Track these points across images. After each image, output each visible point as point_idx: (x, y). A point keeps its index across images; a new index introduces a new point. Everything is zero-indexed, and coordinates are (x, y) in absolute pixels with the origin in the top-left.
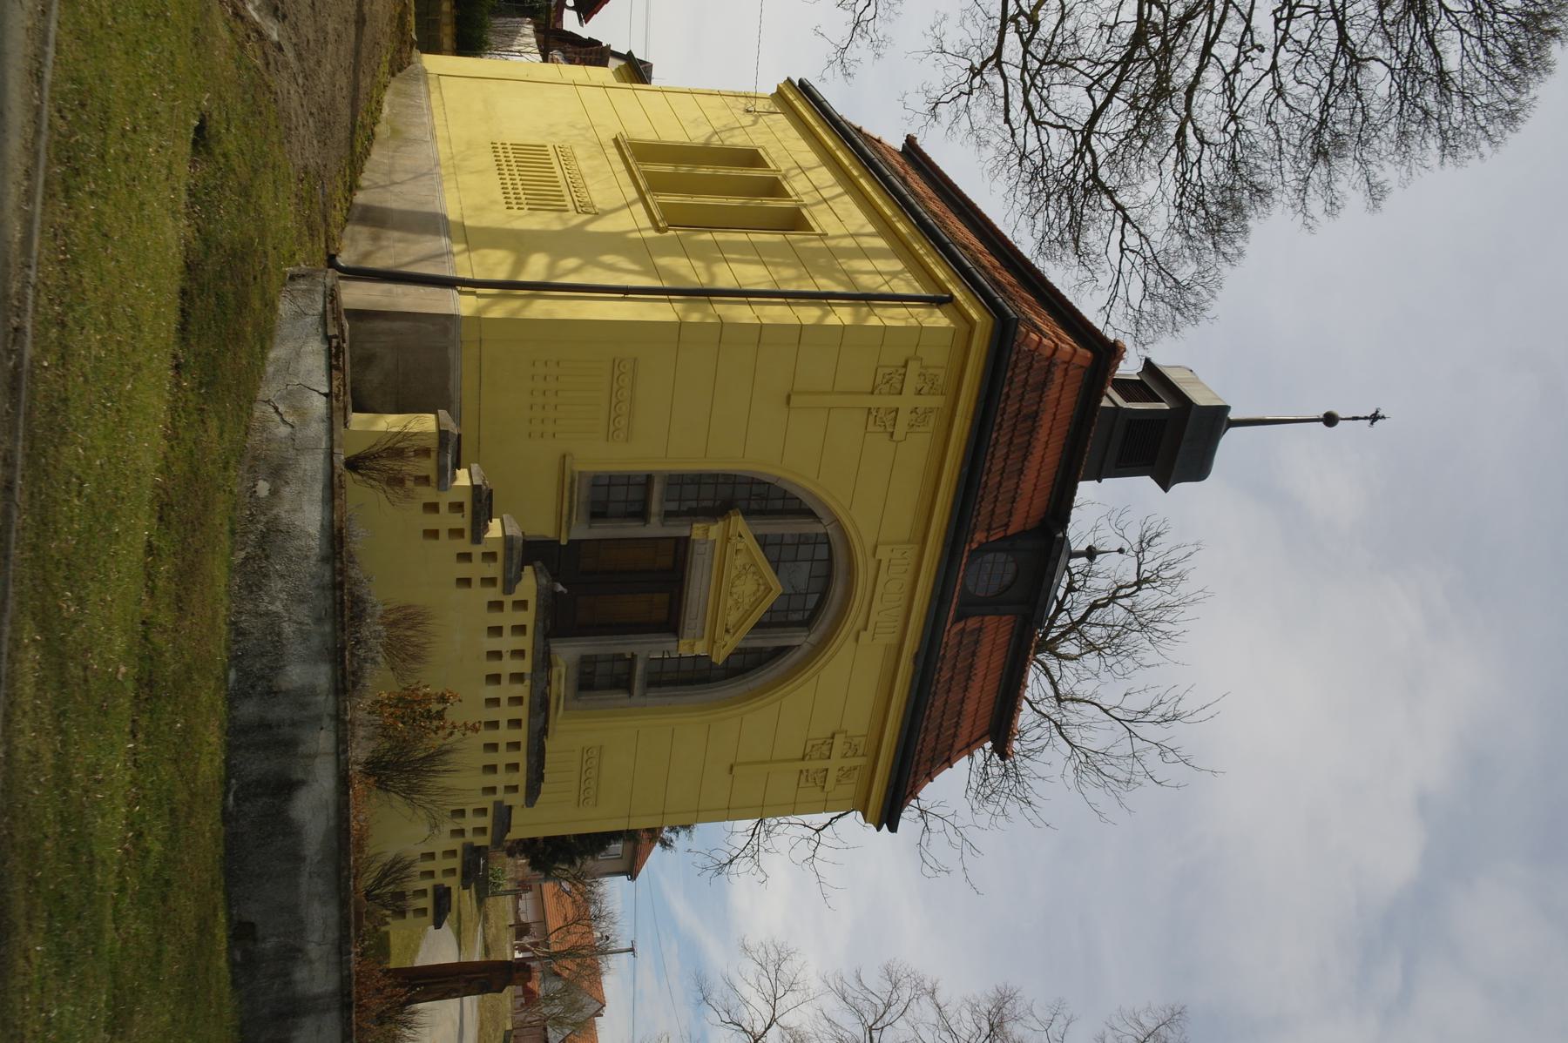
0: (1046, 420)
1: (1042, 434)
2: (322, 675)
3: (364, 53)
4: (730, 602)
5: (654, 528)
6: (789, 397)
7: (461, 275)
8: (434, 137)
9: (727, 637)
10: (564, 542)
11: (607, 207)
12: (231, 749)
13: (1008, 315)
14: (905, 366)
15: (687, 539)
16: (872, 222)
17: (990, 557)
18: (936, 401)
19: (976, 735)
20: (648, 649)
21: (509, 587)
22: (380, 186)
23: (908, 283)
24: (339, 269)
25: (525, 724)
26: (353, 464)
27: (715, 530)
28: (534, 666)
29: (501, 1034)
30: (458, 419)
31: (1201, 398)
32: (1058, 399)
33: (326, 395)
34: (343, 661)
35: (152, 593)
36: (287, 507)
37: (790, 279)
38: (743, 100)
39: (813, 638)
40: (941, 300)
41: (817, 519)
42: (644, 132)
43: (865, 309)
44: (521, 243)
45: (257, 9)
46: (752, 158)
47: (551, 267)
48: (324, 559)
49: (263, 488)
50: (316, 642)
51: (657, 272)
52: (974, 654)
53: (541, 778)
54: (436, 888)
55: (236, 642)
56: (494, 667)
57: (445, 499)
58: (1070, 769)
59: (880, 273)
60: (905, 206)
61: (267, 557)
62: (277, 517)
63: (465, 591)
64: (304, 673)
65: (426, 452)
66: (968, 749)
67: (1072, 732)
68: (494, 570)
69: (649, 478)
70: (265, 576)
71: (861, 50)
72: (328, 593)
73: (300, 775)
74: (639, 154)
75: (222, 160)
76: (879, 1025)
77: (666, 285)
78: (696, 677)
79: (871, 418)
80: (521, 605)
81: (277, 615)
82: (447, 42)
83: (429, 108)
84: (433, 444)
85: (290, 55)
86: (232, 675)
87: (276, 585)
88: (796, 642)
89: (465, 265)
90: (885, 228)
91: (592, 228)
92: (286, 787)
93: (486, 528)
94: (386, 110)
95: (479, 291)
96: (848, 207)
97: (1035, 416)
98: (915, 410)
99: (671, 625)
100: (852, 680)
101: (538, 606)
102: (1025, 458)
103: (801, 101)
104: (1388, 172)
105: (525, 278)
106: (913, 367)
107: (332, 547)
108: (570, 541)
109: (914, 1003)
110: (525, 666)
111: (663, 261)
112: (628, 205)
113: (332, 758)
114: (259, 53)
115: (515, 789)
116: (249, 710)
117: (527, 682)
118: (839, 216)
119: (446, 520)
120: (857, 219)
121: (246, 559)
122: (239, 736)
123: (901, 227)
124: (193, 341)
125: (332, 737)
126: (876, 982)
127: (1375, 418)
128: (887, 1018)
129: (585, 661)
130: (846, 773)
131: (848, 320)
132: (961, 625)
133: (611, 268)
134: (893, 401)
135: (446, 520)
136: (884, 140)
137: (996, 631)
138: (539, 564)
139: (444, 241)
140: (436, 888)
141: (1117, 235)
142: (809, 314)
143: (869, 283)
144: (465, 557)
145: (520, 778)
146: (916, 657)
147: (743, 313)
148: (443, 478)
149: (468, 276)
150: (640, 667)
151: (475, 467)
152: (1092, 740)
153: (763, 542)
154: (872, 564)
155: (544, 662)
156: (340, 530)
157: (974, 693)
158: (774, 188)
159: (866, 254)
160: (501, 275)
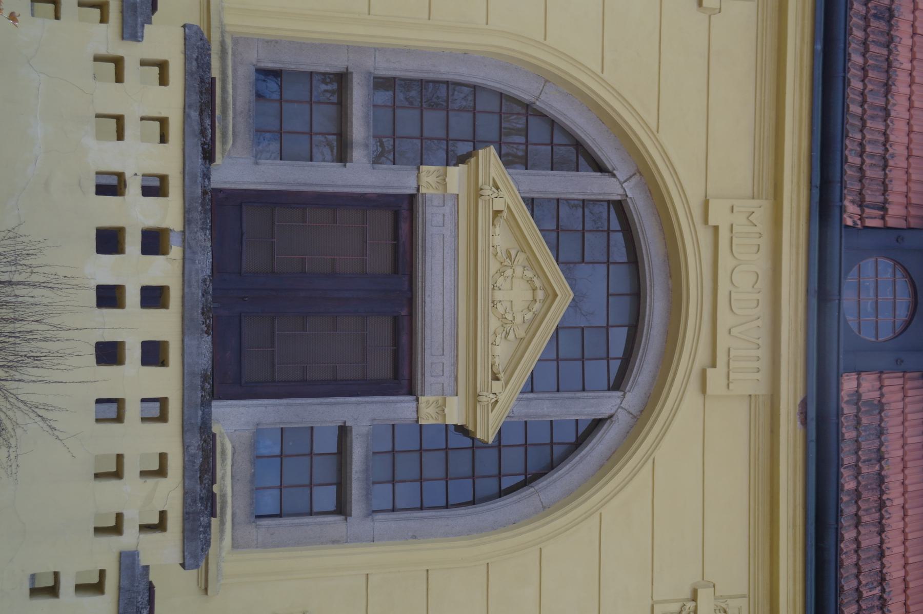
4: (494, 324)
5: (361, 175)
9: (497, 386)
14: (694, 599)
39: (632, 397)
69: (342, 79)
99: (402, 379)
117: (176, 251)
129: (259, 433)
145: (169, 494)
154: (705, 237)
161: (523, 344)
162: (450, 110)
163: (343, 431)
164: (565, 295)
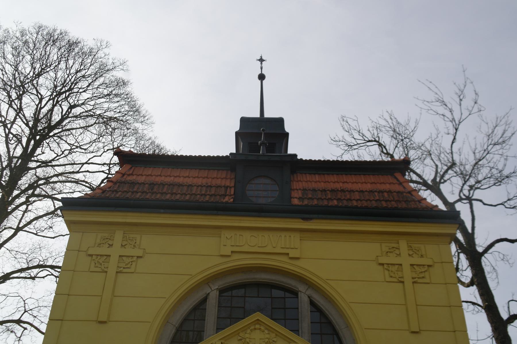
14: (383, 264)
19: (395, 181)
32: (390, 184)
39: (301, 287)
41: (204, 300)
79: (125, 270)
97: (152, 185)
98: (111, 246)
106: (384, 260)
127: (261, 60)
134: (114, 260)
137: (303, 182)
146: (304, 219)
153: (219, 329)
154: (236, 257)
161: (278, 334)
164: (258, 316)
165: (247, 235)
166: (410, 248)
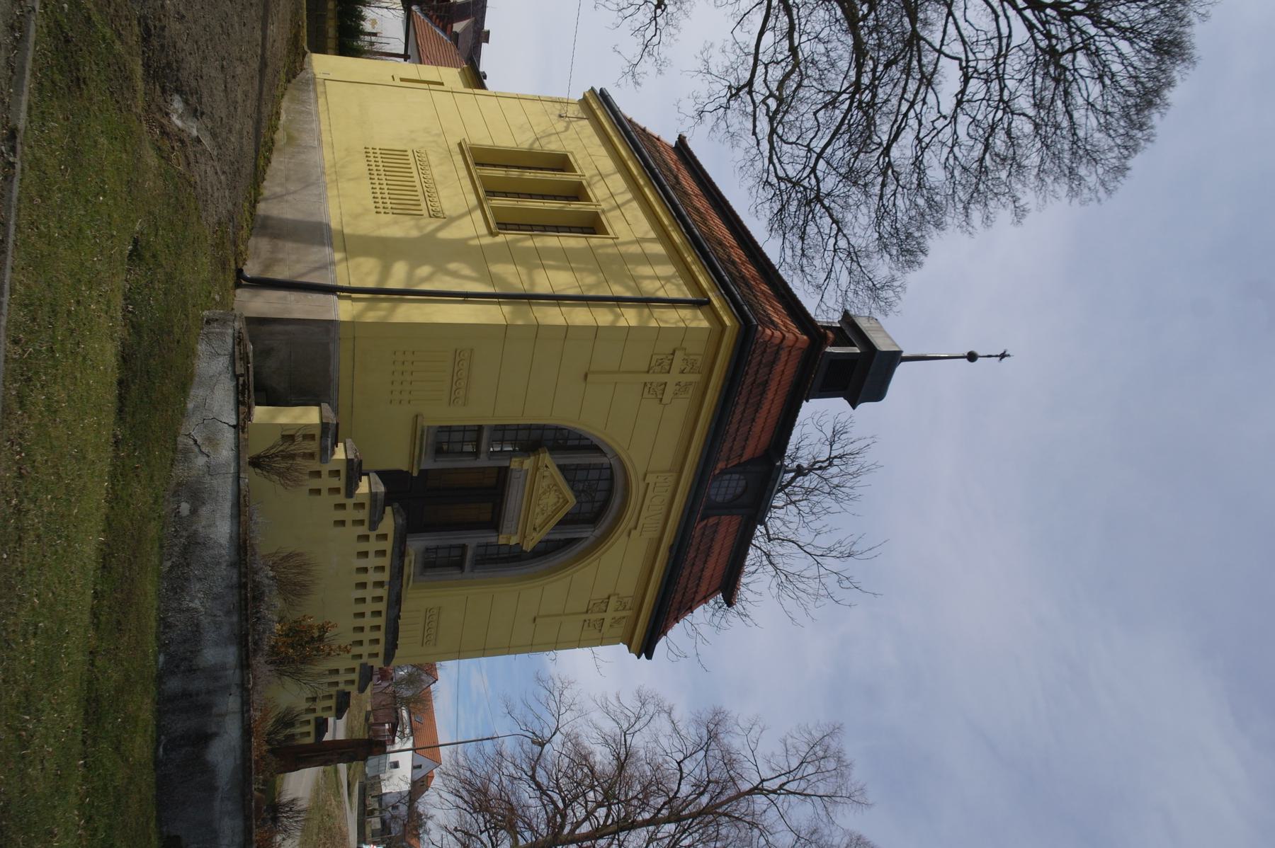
0: (773, 386)
1: (770, 395)
2: (230, 655)
3: (268, 46)
4: (538, 510)
6: (586, 376)
7: (340, 284)
8: (320, 141)
9: (534, 534)
10: (415, 474)
11: (454, 214)
12: (160, 714)
13: (751, 322)
14: (673, 354)
15: (507, 468)
16: (653, 228)
17: (728, 477)
18: (694, 377)
20: (473, 541)
21: (373, 526)
22: (280, 203)
23: (678, 286)
24: (246, 279)
25: (384, 614)
26: (256, 462)
27: (528, 463)
28: (391, 577)
29: (363, 714)
30: (336, 411)
31: (882, 345)
33: (234, 427)
34: (247, 645)
35: (97, 627)
36: (204, 523)
37: (588, 283)
38: (557, 106)
39: (598, 532)
40: (701, 303)
41: (605, 455)
42: (482, 138)
43: (646, 311)
44: (385, 250)
45: (180, 117)
46: (562, 163)
47: (410, 274)
48: (232, 565)
49: (185, 508)
50: (225, 630)
51: (491, 278)
52: (712, 540)
53: (396, 646)
54: (317, 719)
55: (164, 633)
56: (362, 578)
57: (325, 469)
58: (774, 584)
59: (658, 278)
60: (679, 218)
61: (188, 565)
62: (196, 532)
63: (340, 529)
64: (217, 654)
65: (312, 437)
66: (705, 599)
67: (776, 560)
68: (363, 514)
69: (480, 428)
70: (187, 580)
71: (647, 65)
72: (235, 591)
73: (214, 729)
74: (480, 158)
75: (152, 261)
76: (631, 730)
77: (498, 291)
78: (513, 558)
80: (383, 537)
81: (196, 610)
82: (331, 43)
83: (317, 112)
84: (317, 432)
85: (206, 141)
86: (161, 658)
87: (196, 586)
88: (584, 535)
89: (343, 275)
90: (664, 237)
91: (443, 235)
92: (203, 738)
93: (357, 486)
94: (283, 117)
95: (354, 295)
96: (634, 211)
99: (494, 524)
100: (623, 563)
101: (395, 538)
102: (756, 411)
103: (600, 104)
104: (1028, 197)
105: (391, 284)
106: (679, 354)
107: (239, 554)
108: (421, 472)
109: (656, 717)
110: (385, 577)
111: (497, 269)
112: (470, 212)
113: (238, 716)
114: (182, 160)
115: (376, 655)
116: (174, 684)
117: (386, 587)
118: (630, 223)
119: (326, 482)
120: (643, 227)
121: (172, 567)
122: (166, 705)
123: (676, 237)
124: (128, 419)
125: (239, 700)
126: (631, 703)
127: (1003, 356)
128: (637, 727)
130: (617, 621)
131: (633, 323)
132: (703, 523)
133: (455, 274)
135: (326, 482)
136: (662, 138)
137: (728, 526)
138: (396, 505)
139: (327, 250)
140: (317, 719)
141: (832, 241)
142: (603, 317)
143: (651, 288)
144: (342, 506)
145: (380, 649)
146: (671, 548)
147: (553, 316)
148: (325, 453)
149: (345, 284)
150: (469, 554)
151: (349, 442)
152: (791, 565)
153: (562, 468)
154: (642, 486)
155: (400, 552)
156: (245, 541)
157: (712, 560)
158: (578, 192)
159: (648, 259)
160: (370, 283)
162: (535, 439)
163: (464, 547)
164: (572, 500)
165: (667, 495)
166: (688, 384)
